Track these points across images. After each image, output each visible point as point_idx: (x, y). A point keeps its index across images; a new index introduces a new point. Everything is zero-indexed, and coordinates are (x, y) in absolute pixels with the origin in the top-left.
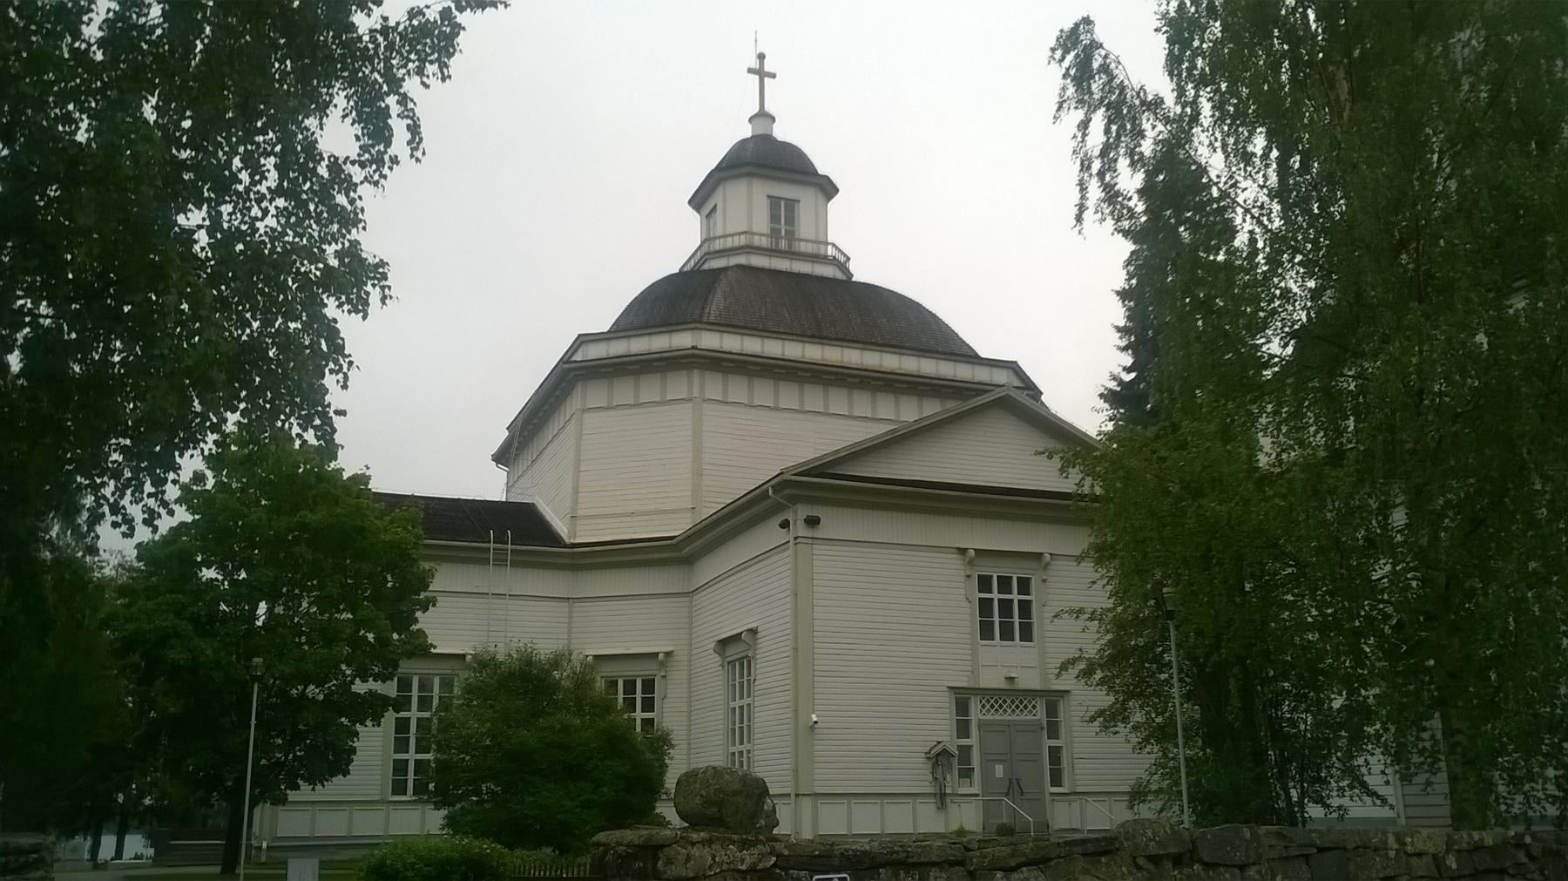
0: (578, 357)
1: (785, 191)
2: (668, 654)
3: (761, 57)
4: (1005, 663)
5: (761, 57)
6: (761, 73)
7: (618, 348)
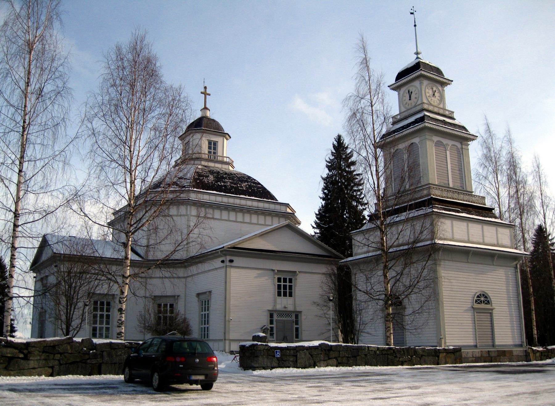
1: (214, 138)
2: (178, 296)
3: (205, 88)
4: (284, 303)
5: (205, 88)
6: (205, 93)
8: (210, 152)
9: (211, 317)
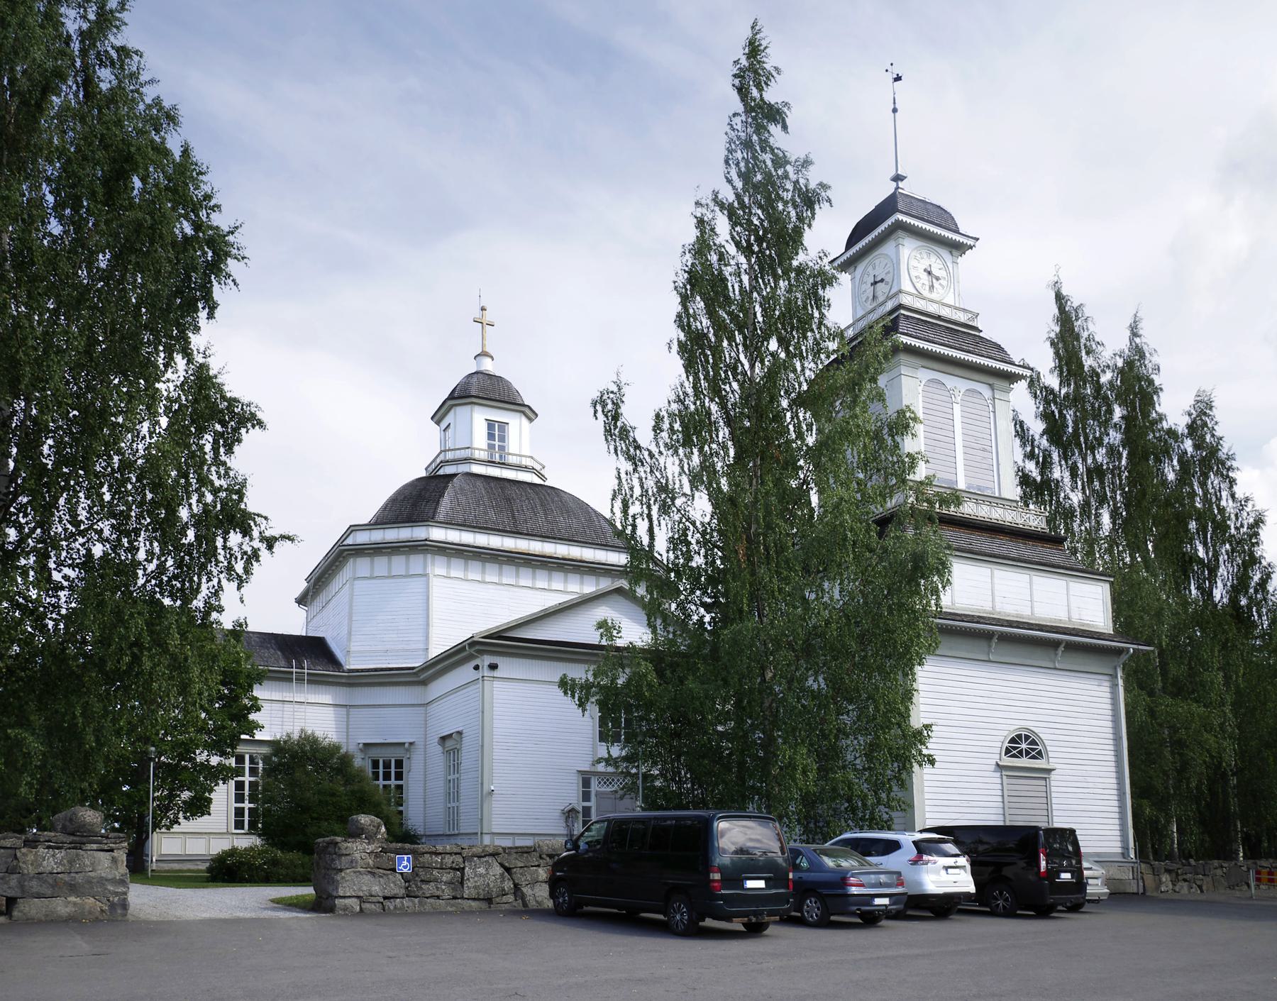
0: (349, 541)
2: (411, 744)
7: (378, 536)
8: (491, 447)
9: (463, 785)
